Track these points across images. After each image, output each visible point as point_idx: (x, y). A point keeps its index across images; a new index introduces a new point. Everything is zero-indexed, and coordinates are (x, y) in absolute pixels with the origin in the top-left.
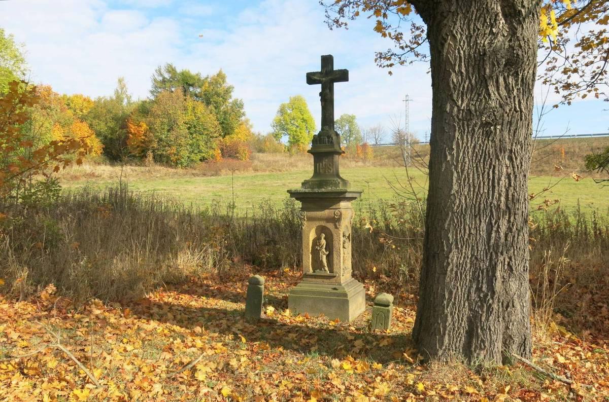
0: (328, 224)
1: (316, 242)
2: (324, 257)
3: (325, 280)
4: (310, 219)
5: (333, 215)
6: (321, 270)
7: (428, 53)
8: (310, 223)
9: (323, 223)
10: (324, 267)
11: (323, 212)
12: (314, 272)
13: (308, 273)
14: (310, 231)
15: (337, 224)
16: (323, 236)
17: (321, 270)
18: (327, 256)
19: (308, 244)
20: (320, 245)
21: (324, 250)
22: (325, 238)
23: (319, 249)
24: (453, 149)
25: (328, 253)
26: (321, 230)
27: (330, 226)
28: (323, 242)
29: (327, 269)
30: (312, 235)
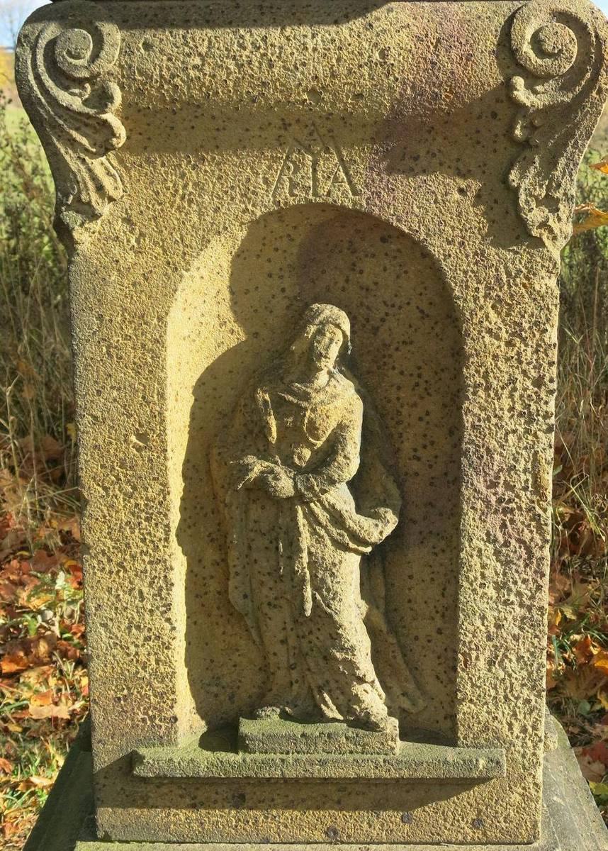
0: (403, 184)
1: (249, 400)
2: (350, 567)
3: (344, 820)
4: (176, 127)
5: (488, 72)
6: (314, 715)
7: (55, 778)
8: (174, 173)
9: (337, 180)
10: (342, 681)
11: (345, 31)
12: (223, 733)
13: (154, 758)
14: (174, 269)
15: (525, 182)
16: (335, 327)
17: (314, 715)
18: (366, 561)
19: (149, 436)
20: (297, 433)
21: (341, 498)
22: (349, 364)
23: (285, 484)
24: (543, 575)
25: (391, 522)
26: (305, 261)
27: (437, 209)
28: (338, 402)
29: (373, 699)
30: (195, 327)
